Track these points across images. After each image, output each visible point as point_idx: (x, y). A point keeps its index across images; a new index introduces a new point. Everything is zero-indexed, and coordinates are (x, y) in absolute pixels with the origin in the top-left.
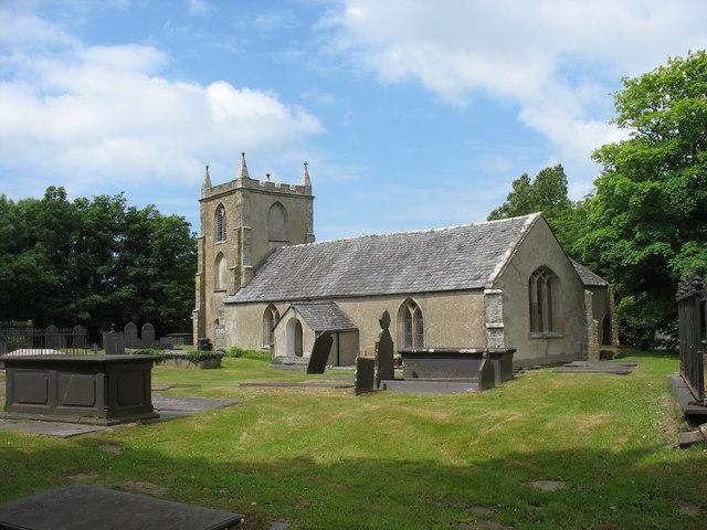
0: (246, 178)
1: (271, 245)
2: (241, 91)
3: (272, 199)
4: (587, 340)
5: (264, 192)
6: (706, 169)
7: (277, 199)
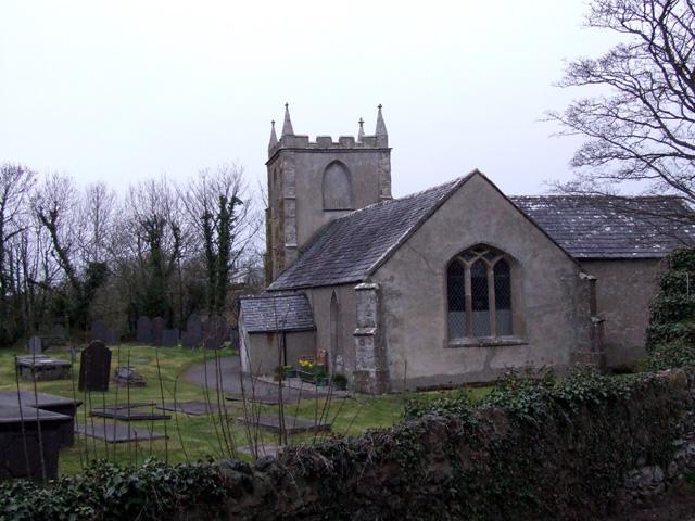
5: (315, 151)
7: (333, 157)
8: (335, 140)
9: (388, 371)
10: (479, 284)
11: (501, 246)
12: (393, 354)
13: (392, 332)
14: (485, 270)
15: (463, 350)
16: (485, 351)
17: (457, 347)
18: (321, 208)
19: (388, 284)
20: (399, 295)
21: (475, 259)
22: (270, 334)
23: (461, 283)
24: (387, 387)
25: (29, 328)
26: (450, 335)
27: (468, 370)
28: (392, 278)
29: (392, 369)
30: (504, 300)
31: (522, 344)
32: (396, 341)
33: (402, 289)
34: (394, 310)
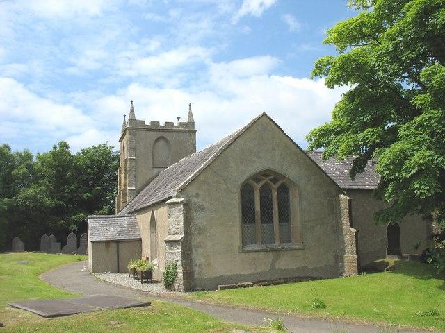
0: (132, 120)
1: (156, 171)
2: (345, 95)
3: (156, 135)
4: (343, 251)
5: (149, 130)
6: (444, 75)
7: (160, 134)
8: (162, 124)
9: (193, 272)
10: (266, 205)
11: (283, 171)
12: (198, 258)
13: (196, 239)
14: (270, 192)
15: (253, 254)
16: (271, 256)
17: (249, 251)
18: (151, 166)
19: (194, 200)
20: (203, 209)
21: (265, 181)
22: (107, 243)
23: (253, 200)
24: (193, 285)
25: (229, 299)
26: (244, 243)
27: (259, 270)
28: (197, 195)
29: (196, 270)
30: (285, 217)
31: (299, 249)
32: (200, 247)
33: (206, 204)
34: (198, 221)
